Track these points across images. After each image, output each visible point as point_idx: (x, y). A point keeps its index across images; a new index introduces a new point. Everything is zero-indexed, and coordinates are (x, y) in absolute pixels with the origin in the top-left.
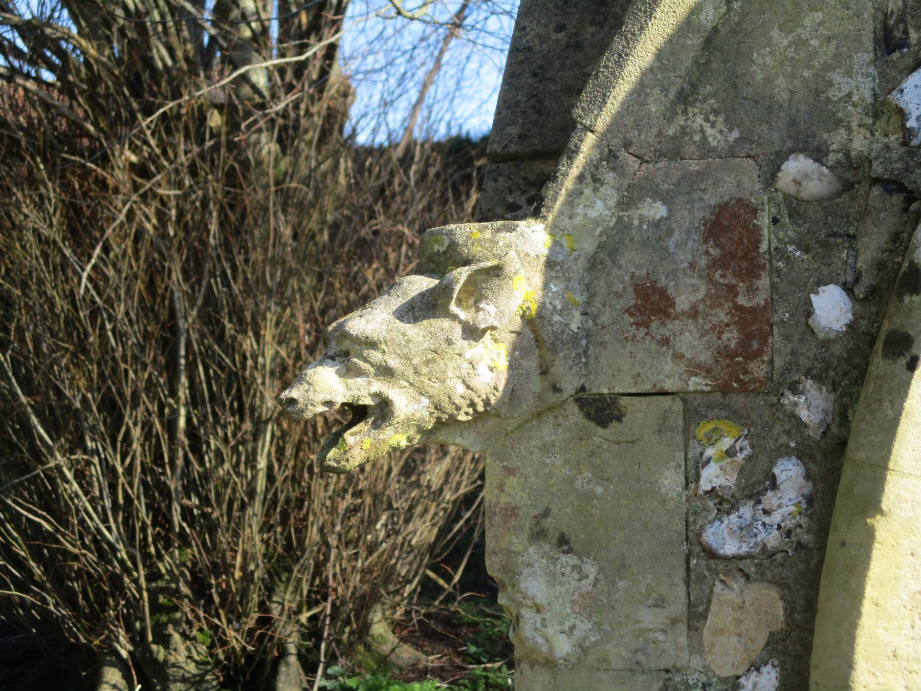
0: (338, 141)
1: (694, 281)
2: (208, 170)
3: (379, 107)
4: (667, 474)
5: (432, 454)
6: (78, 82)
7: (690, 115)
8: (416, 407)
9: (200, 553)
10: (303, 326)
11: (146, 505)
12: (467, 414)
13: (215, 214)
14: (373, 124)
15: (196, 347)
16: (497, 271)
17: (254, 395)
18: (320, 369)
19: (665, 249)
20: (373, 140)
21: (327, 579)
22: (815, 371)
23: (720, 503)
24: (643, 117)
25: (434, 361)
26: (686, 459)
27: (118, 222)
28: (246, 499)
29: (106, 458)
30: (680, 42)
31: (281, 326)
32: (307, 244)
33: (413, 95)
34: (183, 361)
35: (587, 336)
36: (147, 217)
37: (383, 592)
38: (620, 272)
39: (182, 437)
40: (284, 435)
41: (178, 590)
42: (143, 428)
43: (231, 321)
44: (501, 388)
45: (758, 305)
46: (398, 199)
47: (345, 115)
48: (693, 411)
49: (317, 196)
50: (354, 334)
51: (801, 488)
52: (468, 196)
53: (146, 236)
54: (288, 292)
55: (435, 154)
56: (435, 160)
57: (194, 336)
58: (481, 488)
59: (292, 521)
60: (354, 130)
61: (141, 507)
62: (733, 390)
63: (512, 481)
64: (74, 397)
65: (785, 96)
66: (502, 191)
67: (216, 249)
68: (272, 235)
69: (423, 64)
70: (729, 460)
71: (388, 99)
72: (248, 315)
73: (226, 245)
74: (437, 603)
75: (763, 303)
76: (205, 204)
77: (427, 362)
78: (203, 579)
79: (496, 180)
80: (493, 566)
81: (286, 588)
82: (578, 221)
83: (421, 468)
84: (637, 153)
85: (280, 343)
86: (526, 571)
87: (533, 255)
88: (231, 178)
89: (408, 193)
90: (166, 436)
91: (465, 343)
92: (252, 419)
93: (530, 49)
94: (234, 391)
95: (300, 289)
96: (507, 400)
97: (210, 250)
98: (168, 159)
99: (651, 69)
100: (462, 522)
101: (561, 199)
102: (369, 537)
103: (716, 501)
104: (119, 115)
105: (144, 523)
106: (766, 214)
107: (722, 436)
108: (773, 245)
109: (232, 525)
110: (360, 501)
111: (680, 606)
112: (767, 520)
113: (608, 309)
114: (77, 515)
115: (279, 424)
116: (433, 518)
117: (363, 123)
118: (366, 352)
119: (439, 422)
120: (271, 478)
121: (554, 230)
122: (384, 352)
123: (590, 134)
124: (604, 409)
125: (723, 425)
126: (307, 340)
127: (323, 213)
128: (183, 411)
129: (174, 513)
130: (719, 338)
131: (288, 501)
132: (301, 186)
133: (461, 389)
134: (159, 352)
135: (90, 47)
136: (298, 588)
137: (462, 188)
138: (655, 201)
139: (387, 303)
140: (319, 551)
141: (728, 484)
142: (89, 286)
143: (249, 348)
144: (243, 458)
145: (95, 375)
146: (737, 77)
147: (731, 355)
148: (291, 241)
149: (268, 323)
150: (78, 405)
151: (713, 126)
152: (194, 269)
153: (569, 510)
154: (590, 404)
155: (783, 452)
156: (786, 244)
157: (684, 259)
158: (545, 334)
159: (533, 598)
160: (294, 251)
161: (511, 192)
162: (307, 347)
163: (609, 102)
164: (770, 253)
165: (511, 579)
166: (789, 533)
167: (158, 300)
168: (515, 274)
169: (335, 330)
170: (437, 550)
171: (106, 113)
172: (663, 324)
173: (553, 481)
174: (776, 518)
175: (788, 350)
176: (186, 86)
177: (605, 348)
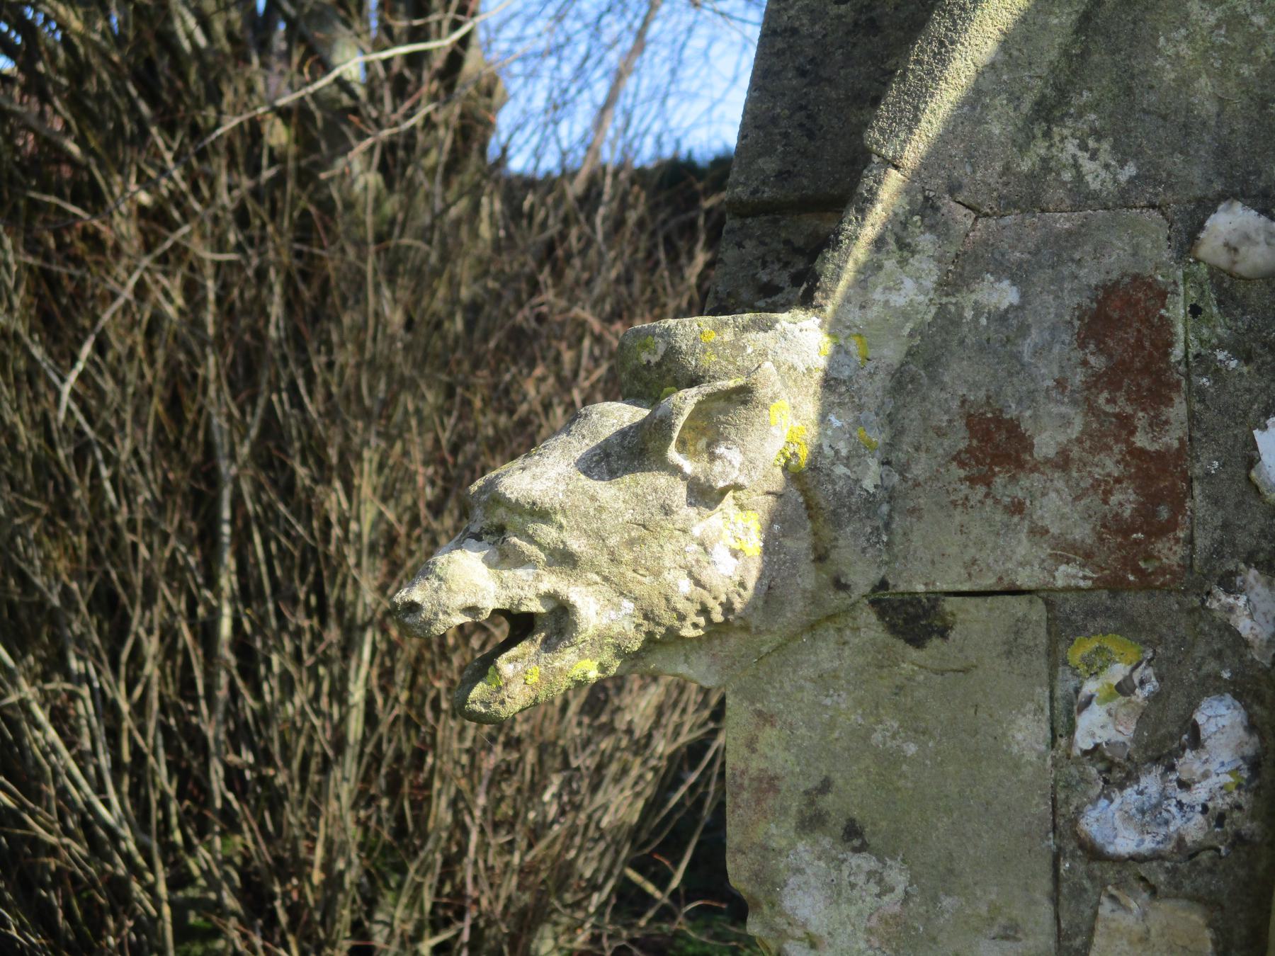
0: (479, 170)
1: (1063, 409)
2: (266, 218)
3: (546, 111)
4: (1022, 722)
5: (634, 682)
6: (52, 74)
7: (1057, 138)
8: (613, 615)
9: (255, 842)
10: (423, 473)
11: (168, 764)
12: (695, 626)
13: (278, 289)
14: (535, 140)
15: (250, 506)
16: (743, 395)
17: (343, 585)
18: (457, 554)
19: (1017, 356)
20: (536, 168)
21: (463, 884)
22: (1261, 556)
23: (1109, 770)
24: (980, 143)
25: (642, 540)
26: (1052, 698)
27: (121, 301)
28: (330, 753)
29: (101, 689)
30: (1040, 21)
31: (386, 471)
32: (429, 337)
33: (601, 90)
34: (226, 529)
35: (891, 499)
36: (167, 294)
37: (556, 904)
38: (943, 395)
39: (226, 653)
40: (393, 647)
41: (219, 903)
42: (162, 639)
43: (304, 463)
44: (751, 583)
45: (1169, 448)
46: (577, 262)
47: (489, 126)
48: (1063, 620)
49: (445, 258)
50: (513, 497)
51: (1240, 745)
52: (691, 257)
53: (166, 325)
54: (398, 417)
55: (636, 189)
56: (637, 198)
57: (246, 488)
58: (714, 733)
59: (406, 788)
60: (504, 150)
61: (164, 780)
62: (1129, 586)
63: (769, 735)
64: (50, 588)
65: (1211, 107)
66: (750, 263)
67: (279, 345)
68: (371, 322)
69: (617, 41)
70: (1122, 699)
71: (559, 101)
72: (333, 455)
73: (296, 338)
74: (643, 923)
75: (1176, 444)
76: (261, 274)
77: (631, 543)
78: (260, 885)
79: (740, 245)
80: (738, 872)
81: (397, 900)
82: (874, 312)
83: (616, 702)
84: (971, 201)
85: (384, 499)
86: (793, 881)
87: (802, 368)
88: (304, 229)
89: (592, 253)
90: (200, 652)
91: (692, 512)
92: (340, 623)
93: (794, 31)
94: (310, 578)
95: (418, 411)
96: (760, 603)
97: (270, 347)
98: (201, 200)
99: (992, 66)
100: (683, 789)
101: (847, 276)
102: (532, 815)
103: (1101, 766)
104: (120, 127)
105: (164, 794)
106: (1181, 299)
107: (1111, 661)
108: (1193, 351)
109: (309, 796)
110: (515, 755)
111: (1042, 938)
112: (1185, 797)
113: (923, 455)
114: (55, 781)
115: (384, 631)
116: (636, 783)
117: (519, 139)
118: (531, 528)
119: (650, 639)
120: (371, 719)
121: (836, 328)
122: (561, 527)
123: (893, 172)
124: (916, 618)
125: (1112, 643)
126: (429, 493)
127: (454, 284)
128: (227, 610)
129: (213, 777)
130: (1105, 502)
131: (399, 757)
132: (418, 243)
133: (685, 586)
134: (188, 515)
135: (72, 16)
136: (416, 898)
137: (682, 245)
138: (999, 280)
139: (566, 448)
140: (450, 839)
141: (1121, 738)
142: (74, 407)
143: (335, 506)
144: (326, 687)
145: (83, 552)
146: (1132, 77)
147: (1124, 530)
148: (401, 332)
149: (366, 466)
150: (56, 601)
151: (1093, 157)
152: (245, 375)
153: (861, 781)
154: (894, 609)
155: (1210, 686)
156: (1213, 348)
157: (1046, 373)
158: (823, 496)
159: (804, 925)
160: (407, 348)
161: (764, 265)
162: (429, 505)
163: (924, 119)
164: (1187, 364)
165: (769, 893)
166: (1220, 819)
167: (187, 429)
168: (773, 399)
169: (482, 490)
170: (644, 836)
171: (98, 124)
172: (1013, 479)
173: (836, 735)
174: (1200, 794)
175: (1218, 522)
176: (230, 80)
177: (920, 518)
